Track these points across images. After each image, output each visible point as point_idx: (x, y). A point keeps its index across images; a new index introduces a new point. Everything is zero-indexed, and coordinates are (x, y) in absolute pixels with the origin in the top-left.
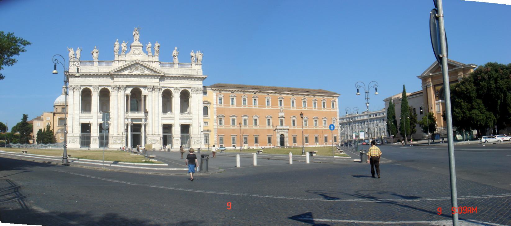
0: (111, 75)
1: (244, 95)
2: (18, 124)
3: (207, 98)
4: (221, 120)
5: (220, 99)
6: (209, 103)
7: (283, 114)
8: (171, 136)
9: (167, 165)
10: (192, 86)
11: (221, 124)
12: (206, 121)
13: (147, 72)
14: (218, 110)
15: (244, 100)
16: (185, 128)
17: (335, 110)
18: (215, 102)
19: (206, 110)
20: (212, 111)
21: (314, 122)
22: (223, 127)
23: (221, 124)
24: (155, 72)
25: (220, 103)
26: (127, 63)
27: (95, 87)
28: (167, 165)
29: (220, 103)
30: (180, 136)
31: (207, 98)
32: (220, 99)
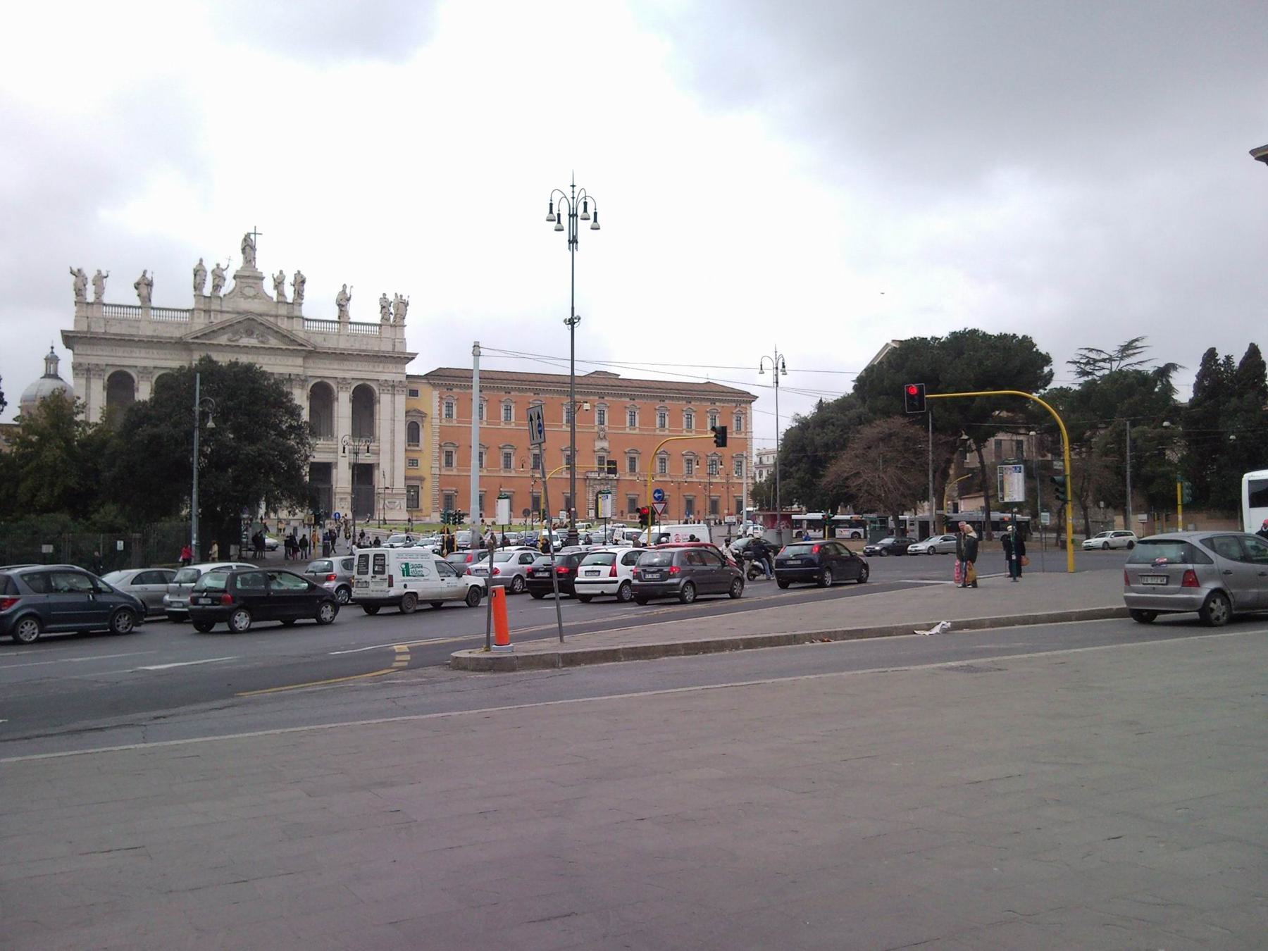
0: (186, 343)
1: (508, 396)
2: (934, 339)
3: (416, 403)
4: (449, 455)
5: (449, 406)
6: (422, 415)
7: (605, 444)
8: (330, 489)
9: (279, 623)
10: (383, 377)
11: (449, 463)
12: (414, 456)
13: (273, 342)
14: (443, 431)
15: (508, 409)
16: (363, 474)
17: (743, 436)
18: (436, 412)
19: (413, 433)
20: (429, 438)
21: (685, 465)
22: (455, 472)
23: (449, 463)
24: (293, 341)
25: (449, 415)
26: (227, 317)
27: (145, 371)
28: (279, 623)
29: (449, 415)
30: (350, 490)
31: (416, 403)
32: (449, 406)
